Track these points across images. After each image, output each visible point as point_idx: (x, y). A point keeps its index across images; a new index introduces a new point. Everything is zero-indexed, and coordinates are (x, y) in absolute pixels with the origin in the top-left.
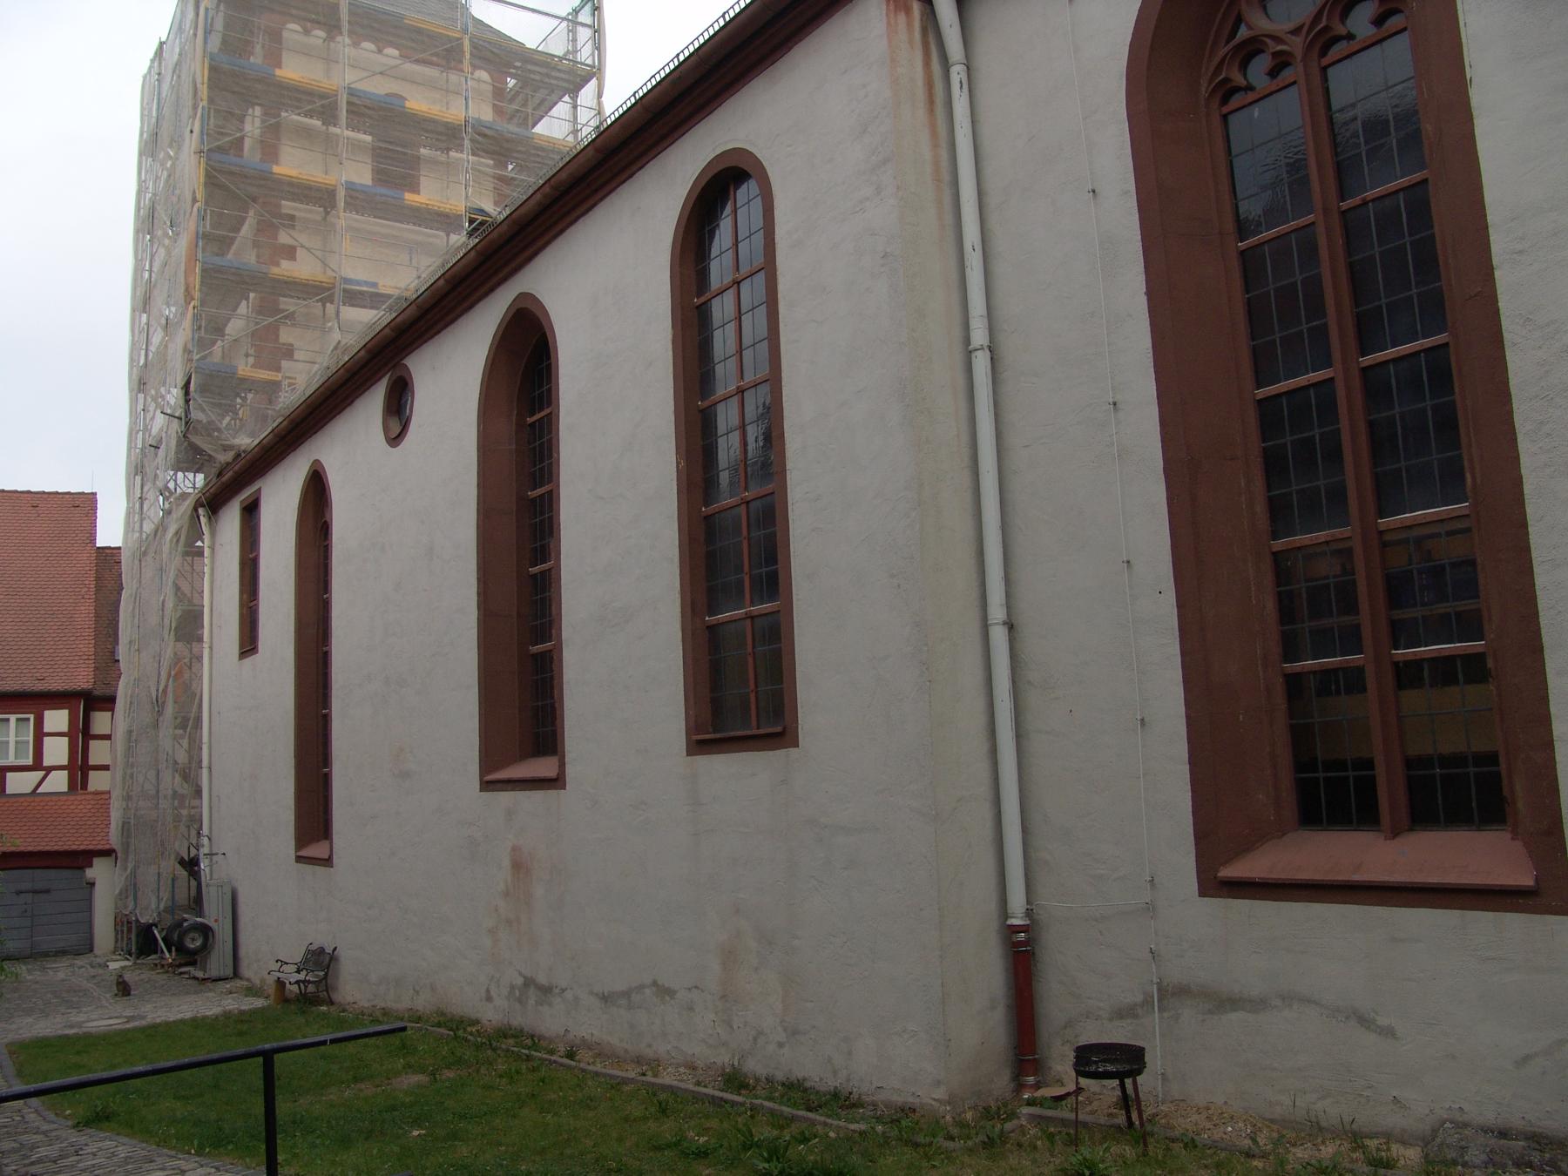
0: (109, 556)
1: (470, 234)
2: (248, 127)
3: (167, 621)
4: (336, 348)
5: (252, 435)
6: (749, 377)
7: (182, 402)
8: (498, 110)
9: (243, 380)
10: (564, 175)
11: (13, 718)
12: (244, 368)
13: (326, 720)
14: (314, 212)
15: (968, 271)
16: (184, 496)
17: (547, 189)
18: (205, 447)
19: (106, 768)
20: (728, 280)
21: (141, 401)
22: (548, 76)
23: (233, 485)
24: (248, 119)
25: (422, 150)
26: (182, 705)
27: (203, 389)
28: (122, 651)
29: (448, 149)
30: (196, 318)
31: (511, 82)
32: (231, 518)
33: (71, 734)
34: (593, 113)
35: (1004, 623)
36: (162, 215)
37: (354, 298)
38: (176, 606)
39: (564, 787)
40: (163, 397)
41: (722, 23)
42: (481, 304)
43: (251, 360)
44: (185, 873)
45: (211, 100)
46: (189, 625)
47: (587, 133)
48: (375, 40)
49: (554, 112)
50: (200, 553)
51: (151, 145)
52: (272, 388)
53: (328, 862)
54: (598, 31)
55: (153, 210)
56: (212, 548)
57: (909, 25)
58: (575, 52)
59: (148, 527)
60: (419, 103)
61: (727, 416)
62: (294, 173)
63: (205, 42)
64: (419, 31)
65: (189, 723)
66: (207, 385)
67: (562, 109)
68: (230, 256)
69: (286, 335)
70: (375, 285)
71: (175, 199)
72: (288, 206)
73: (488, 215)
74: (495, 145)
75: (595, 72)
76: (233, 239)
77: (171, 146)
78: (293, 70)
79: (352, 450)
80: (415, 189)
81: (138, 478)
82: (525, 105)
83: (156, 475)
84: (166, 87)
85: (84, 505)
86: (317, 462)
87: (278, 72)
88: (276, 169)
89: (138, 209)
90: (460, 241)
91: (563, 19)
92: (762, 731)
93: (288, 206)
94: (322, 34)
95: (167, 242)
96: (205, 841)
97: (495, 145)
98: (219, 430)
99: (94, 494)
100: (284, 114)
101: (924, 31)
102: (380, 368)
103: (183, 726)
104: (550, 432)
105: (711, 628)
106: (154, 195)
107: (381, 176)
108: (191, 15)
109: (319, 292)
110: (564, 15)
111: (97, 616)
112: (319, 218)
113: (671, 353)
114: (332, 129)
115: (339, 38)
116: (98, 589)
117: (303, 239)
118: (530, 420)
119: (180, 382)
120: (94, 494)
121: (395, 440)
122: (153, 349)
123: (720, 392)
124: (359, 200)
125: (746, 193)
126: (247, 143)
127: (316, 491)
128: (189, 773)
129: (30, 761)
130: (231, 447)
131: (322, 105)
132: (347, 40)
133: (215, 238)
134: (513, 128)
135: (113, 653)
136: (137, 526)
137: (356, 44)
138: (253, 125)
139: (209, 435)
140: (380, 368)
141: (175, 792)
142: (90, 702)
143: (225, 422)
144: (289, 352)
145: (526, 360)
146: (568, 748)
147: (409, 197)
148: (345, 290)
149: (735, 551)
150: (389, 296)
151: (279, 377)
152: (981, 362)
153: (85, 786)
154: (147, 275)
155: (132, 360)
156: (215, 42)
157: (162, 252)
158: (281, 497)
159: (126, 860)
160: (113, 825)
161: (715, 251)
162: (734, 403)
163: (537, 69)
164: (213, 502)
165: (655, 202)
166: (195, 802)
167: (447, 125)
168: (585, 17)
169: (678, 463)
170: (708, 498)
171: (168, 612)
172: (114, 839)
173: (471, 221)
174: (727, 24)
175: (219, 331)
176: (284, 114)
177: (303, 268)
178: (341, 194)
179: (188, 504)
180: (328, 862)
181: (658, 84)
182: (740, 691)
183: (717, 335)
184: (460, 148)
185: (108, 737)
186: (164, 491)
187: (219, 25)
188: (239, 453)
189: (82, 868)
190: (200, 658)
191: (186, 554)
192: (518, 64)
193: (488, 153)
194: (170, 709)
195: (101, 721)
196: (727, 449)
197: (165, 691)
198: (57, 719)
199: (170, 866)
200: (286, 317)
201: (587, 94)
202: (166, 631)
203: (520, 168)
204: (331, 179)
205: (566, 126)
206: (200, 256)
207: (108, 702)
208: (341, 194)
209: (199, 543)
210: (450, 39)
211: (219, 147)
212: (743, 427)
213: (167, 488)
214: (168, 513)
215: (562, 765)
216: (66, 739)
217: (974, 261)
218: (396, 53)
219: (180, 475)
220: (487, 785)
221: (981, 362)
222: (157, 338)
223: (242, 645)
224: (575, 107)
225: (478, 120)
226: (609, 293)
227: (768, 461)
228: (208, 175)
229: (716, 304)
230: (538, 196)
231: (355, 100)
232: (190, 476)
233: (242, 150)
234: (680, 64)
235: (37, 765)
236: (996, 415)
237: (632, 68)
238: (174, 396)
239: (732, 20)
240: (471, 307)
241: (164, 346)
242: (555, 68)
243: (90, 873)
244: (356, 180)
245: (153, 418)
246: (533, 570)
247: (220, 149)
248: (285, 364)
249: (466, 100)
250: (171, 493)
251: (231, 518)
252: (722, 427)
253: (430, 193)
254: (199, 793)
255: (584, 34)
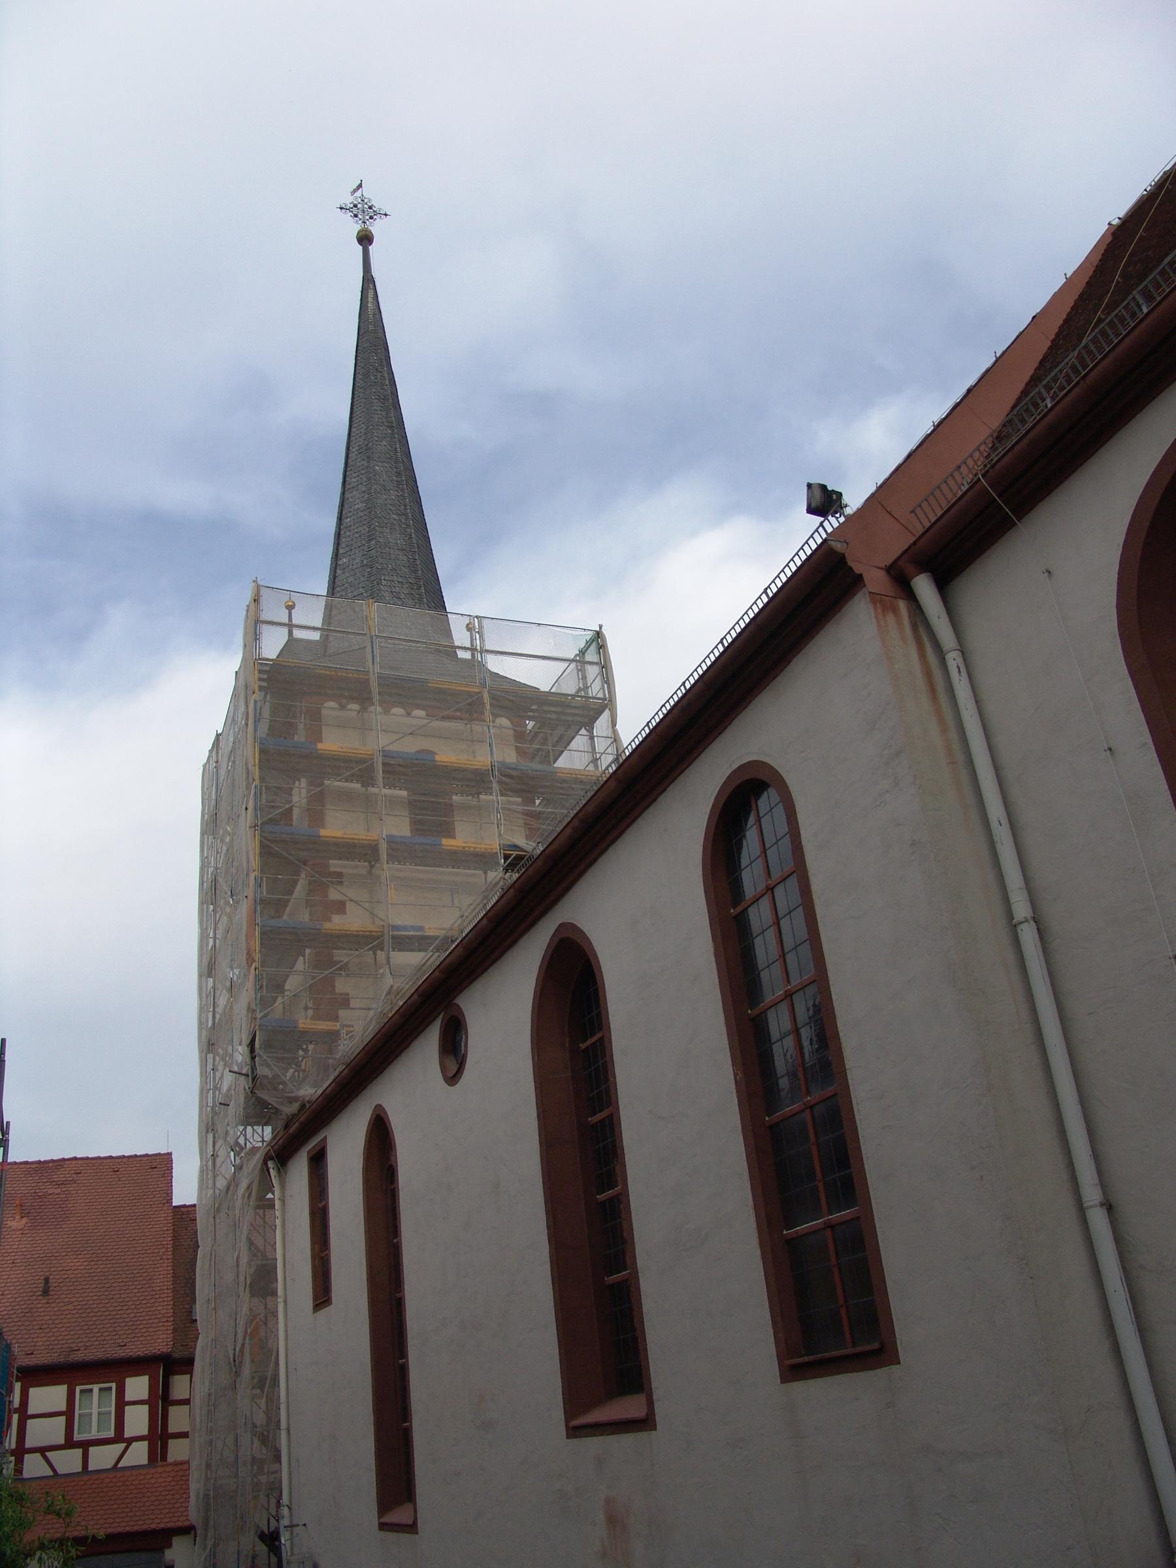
0: (185, 1214)
1: (506, 870)
2: (295, 799)
3: (242, 1278)
4: (389, 993)
5: (315, 1085)
6: (795, 981)
7: (248, 1060)
8: (520, 752)
9: (304, 1033)
10: (590, 808)
11: (96, 1388)
12: (304, 1021)
13: (403, 1370)
14: (361, 867)
15: (999, 846)
16: (254, 1150)
17: (576, 823)
18: (272, 1101)
19: (185, 1435)
20: (761, 887)
21: (210, 1061)
22: (563, 713)
23: (299, 1136)
24: (295, 792)
25: (454, 797)
26: (258, 1363)
27: (268, 1045)
28: (200, 1310)
29: (479, 794)
30: (258, 978)
31: (530, 724)
32: (300, 1167)
33: (150, 1402)
34: (610, 741)
35: (1102, 1205)
36: (224, 886)
37: (403, 943)
38: (249, 1263)
39: (654, 1428)
40: (231, 1056)
41: (721, 649)
42: (525, 937)
43: (310, 1013)
44: (265, 1548)
45: (262, 779)
46: (263, 1281)
47: (607, 763)
48: (401, 705)
49: (573, 745)
50: (271, 1205)
51: (212, 824)
52: (333, 1036)
53: (412, 1528)
54: (605, 667)
55: (215, 881)
56: (283, 1200)
57: (899, 623)
58: (586, 688)
59: (221, 1183)
60: (447, 755)
61: (778, 1022)
62: (339, 834)
63: (255, 730)
64: (441, 691)
65: (266, 1383)
66: (271, 1041)
67: (580, 741)
68: (285, 917)
69: (342, 985)
70: (421, 928)
71: (234, 870)
72: (335, 865)
73: (522, 850)
74: (521, 784)
75: (607, 704)
76: (288, 901)
77: (228, 823)
78: (332, 742)
79: (412, 1093)
80: (451, 834)
81: (210, 1136)
82: (545, 741)
83: (227, 1133)
84: (223, 773)
85: (159, 1166)
86: (379, 1107)
87: (319, 746)
88: (323, 832)
89: (202, 883)
90: (498, 878)
91: (572, 661)
92: (859, 1349)
93: (335, 865)
94: (356, 707)
95: (228, 910)
96: (285, 1511)
97: (521, 784)
98: (284, 1083)
99: (170, 1154)
100: (327, 782)
101: (914, 626)
102: (434, 1011)
103: (261, 1386)
104: (604, 1056)
105: (789, 1242)
106: (216, 868)
107: (418, 827)
108: (242, 708)
109: (370, 941)
110: (572, 657)
111: (175, 1276)
112: (364, 872)
113: (714, 965)
114: (372, 790)
115: (372, 708)
116: (176, 1247)
117: (351, 893)
118: (583, 1046)
119: (246, 1040)
120: (170, 1154)
121: (452, 1079)
122: (219, 1010)
123: (769, 998)
124: (399, 851)
125: (767, 801)
126: (296, 813)
127: (380, 1136)
128: (267, 1436)
129: (111, 1433)
130: (295, 1099)
131: (359, 769)
132: (379, 709)
133: (271, 903)
134: (536, 766)
135: (191, 1312)
136: (211, 1182)
137: (386, 712)
138: (300, 794)
139: (275, 1089)
140: (434, 1011)
141: (253, 1458)
142: (170, 1365)
143: (289, 1074)
144: (345, 1002)
145: (574, 995)
146: (654, 1384)
147: (447, 842)
148: (393, 937)
149: (804, 1151)
150: (435, 938)
151: (337, 1026)
152: (1028, 935)
153: (164, 1457)
154: (211, 942)
155: (200, 1023)
156: (264, 728)
157: (225, 919)
158: (346, 1143)
159: (205, 1537)
160: (193, 1495)
161: (744, 861)
162: (784, 1007)
163: (553, 709)
164: (281, 1155)
165: (678, 828)
166: (275, 1467)
167: (475, 771)
168: (591, 656)
169: (735, 1075)
170: (771, 1108)
171: (242, 1268)
172: (194, 1515)
173: (506, 857)
174: (726, 649)
175: (279, 988)
176: (327, 782)
177: (353, 921)
178: (383, 847)
179: (259, 1156)
180: (412, 1528)
181: (669, 712)
182: (831, 1309)
183: (758, 943)
184: (489, 791)
185: (186, 1402)
186: (236, 1148)
187: (266, 714)
188: (301, 1100)
189: (161, 1550)
190: (275, 1314)
191: (258, 1207)
192: (534, 707)
193: (516, 792)
194: (247, 1371)
195: (180, 1385)
196: (783, 1054)
197: (242, 1351)
198: (138, 1386)
199: (249, 1542)
200: (340, 969)
201: (601, 725)
202: (242, 1288)
203: (547, 802)
204: (373, 835)
205: (587, 758)
206: (258, 920)
207: (185, 1365)
208: (383, 847)
209: (270, 1196)
210: (470, 694)
211: (271, 820)
212: (796, 1031)
213: (237, 1144)
214: (239, 1168)
215: (650, 1403)
216: (146, 1407)
217: (1003, 834)
218: (422, 713)
219: (249, 1129)
220: (574, 1432)
221: (1028, 935)
222: (222, 1001)
223: (315, 1298)
224: (592, 738)
225: (503, 764)
226: (646, 915)
227: (825, 1059)
228: (263, 846)
229: (752, 912)
230: (568, 831)
231: (388, 760)
232: (259, 1129)
233: (291, 820)
234: (688, 691)
235: (119, 1437)
236: (1053, 985)
237: (641, 700)
238: (240, 1054)
239: (730, 645)
240: (514, 942)
241: (230, 1007)
242: (569, 706)
243: (169, 1555)
244: (395, 833)
245: (221, 1078)
246: (593, 1120)
247: (272, 821)
248: (342, 1013)
249: (491, 747)
250: (242, 1149)
251: (300, 1167)
252: (775, 1034)
253: (465, 836)
254: (277, 1458)
255: (592, 671)
